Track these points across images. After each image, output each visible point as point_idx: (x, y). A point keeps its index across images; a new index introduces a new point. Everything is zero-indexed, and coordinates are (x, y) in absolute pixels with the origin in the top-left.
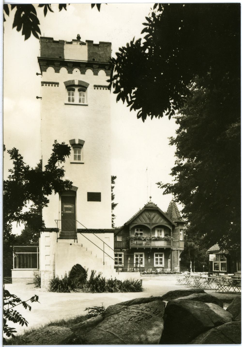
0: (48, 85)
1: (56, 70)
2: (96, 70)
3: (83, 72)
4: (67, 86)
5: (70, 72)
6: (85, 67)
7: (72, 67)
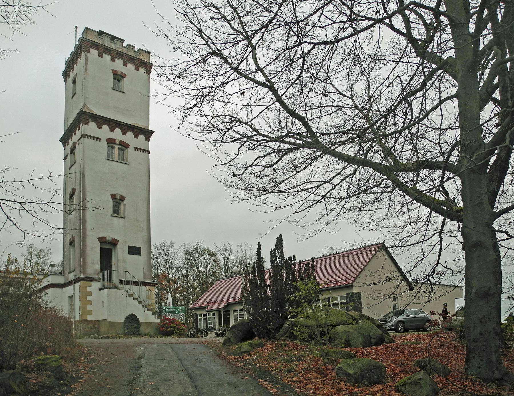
3: (124, 133)
5: (112, 130)
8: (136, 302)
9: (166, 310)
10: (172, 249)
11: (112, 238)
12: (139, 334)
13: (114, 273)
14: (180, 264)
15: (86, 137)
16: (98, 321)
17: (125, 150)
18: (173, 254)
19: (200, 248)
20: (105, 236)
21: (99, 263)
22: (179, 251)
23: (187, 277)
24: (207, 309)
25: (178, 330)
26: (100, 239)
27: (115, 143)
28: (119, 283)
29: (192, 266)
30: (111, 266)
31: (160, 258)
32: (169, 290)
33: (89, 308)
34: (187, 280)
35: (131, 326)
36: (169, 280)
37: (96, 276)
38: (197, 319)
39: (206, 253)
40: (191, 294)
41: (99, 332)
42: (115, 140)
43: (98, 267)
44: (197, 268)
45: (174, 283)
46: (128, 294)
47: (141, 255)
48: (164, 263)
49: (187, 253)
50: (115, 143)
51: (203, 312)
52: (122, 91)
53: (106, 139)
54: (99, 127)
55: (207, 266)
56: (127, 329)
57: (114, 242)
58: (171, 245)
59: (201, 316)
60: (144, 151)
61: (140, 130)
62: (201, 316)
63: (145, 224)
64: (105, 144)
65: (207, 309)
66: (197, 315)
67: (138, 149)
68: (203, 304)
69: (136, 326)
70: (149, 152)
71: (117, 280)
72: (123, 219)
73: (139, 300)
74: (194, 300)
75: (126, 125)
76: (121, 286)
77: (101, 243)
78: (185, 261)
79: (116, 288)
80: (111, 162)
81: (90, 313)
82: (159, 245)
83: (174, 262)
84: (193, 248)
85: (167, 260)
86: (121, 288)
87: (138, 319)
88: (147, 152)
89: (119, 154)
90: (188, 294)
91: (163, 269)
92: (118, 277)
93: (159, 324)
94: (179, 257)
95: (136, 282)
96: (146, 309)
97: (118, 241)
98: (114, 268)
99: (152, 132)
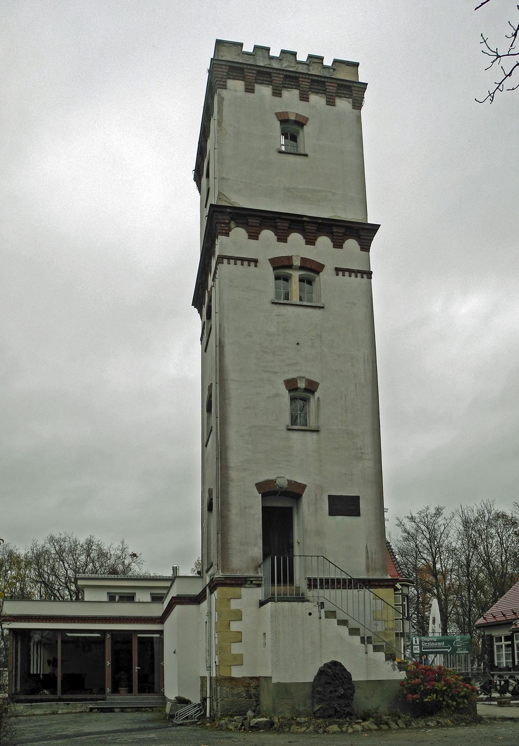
0: (246, 263)
1: (308, 240)
2: (312, 234)
3: (310, 241)
4: (276, 267)
5: (282, 238)
6: (314, 231)
7: (257, 227)
8: (344, 630)
9: (420, 645)
10: (440, 519)
11: (290, 482)
12: (350, 714)
13: (297, 561)
14: (454, 544)
15: (225, 261)
16: (258, 679)
17: (314, 279)
18: (442, 528)
19: (489, 512)
20: (271, 477)
21: (260, 542)
22: (453, 521)
23: (468, 566)
24: (513, 627)
25: (453, 698)
26: (259, 486)
27: (290, 266)
28: (307, 586)
29: (475, 547)
30: (291, 547)
31: (420, 537)
32: (435, 591)
33: (236, 649)
34: (468, 570)
35: (331, 692)
36: (435, 573)
37: (251, 574)
38: (492, 645)
39: (500, 521)
40: (475, 594)
41: (257, 705)
42: (289, 258)
43: (257, 551)
44: (484, 548)
45: (445, 578)
46: (323, 611)
47: (358, 514)
48: (428, 546)
49: (466, 523)
50: (290, 266)
51: (506, 632)
52: (302, 152)
53: (269, 260)
54: (254, 236)
55: (502, 544)
56: (321, 701)
57: (296, 491)
58: (438, 512)
59: (499, 639)
60: (359, 275)
61: (347, 228)
62: (499, 639)
63: (368, 440)
64: (269, 272)
65: (513, 627)
66: (491, 637)
67: (344, 270)
68: (504, 615)
69: (342, 691)
70: (369, 274)
71: (303, 579)
72: (315, 435)
73: (353, 624)
74: (484, 608)
75: (314, 221)
76: (310, 594)
77: (265, 496)
78: (462, 539)
79: (302, 599)
80: (282, 307)
81: (238, 660)
82: (417, 516)
83: (444, 541)
84: (476, 515)
85: (431, 540)
86: (311, 599)
87: (349, 674)
88: (365, 276)
89: (301, 290)
90: (469, 595)
91: (425, 556)
92: (306, 571)
93: (402, 683)
94: (452, 532)
95: (344, 580)
96: (370, 647)
97: (303, 487)
98: (297, 551)
99: (375, 228)
